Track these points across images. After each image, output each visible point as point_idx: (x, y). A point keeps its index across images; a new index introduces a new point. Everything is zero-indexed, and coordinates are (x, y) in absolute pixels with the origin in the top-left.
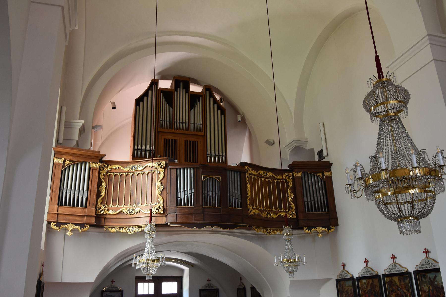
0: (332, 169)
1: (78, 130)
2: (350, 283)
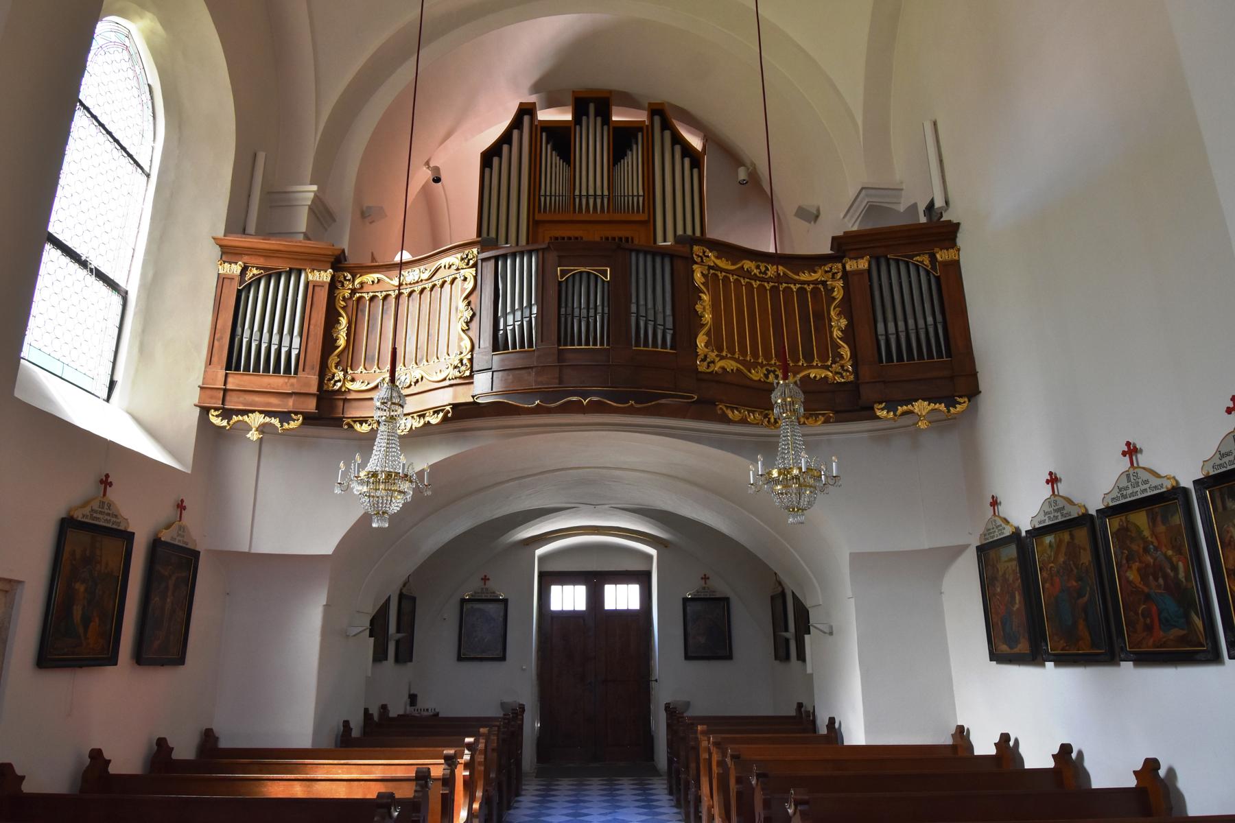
0: (961, 239)
1: (305, 211)
2: (1012, 551)
